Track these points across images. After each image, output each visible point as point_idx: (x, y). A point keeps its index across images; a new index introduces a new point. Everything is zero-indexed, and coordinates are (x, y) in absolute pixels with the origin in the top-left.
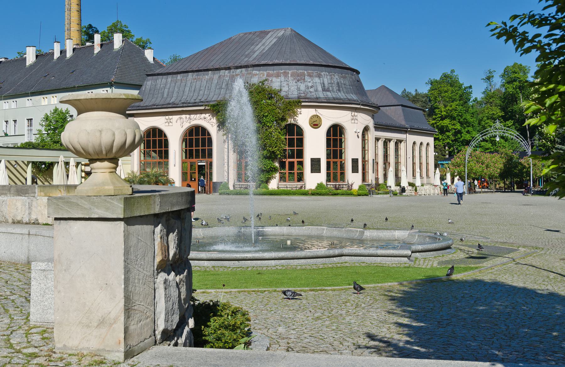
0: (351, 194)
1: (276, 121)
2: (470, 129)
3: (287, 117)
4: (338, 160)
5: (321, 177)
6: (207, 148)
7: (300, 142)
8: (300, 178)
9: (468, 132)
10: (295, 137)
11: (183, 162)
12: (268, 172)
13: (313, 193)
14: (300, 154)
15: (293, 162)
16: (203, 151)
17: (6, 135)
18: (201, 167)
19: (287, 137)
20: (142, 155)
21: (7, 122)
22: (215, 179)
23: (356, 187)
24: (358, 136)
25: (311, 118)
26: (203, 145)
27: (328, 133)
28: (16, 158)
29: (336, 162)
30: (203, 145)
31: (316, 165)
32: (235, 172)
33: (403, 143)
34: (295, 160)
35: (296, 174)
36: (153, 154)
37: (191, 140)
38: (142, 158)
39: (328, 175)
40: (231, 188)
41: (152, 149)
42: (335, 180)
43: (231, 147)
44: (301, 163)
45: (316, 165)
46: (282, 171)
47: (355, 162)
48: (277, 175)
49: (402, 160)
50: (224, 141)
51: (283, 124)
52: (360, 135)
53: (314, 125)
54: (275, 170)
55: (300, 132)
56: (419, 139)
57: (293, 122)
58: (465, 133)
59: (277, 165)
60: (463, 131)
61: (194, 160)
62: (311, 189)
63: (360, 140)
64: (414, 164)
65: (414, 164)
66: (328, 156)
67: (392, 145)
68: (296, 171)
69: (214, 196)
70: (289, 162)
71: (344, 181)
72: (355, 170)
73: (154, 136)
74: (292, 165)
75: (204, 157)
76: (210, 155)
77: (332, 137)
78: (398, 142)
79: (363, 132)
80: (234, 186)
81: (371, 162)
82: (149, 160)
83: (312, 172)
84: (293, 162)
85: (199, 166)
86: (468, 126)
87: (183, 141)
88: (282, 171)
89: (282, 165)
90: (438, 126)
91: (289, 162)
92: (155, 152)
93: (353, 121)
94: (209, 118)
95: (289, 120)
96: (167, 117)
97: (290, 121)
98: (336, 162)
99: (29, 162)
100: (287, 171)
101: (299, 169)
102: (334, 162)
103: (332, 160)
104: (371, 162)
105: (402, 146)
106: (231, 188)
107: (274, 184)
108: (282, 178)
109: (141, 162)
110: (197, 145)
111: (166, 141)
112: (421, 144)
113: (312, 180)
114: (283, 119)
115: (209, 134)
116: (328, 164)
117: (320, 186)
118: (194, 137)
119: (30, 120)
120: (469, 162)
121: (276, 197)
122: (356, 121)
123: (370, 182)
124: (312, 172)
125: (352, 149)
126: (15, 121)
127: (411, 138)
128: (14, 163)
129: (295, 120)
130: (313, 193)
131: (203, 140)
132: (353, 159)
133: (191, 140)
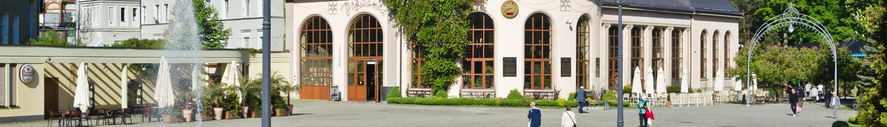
0: (555, 105)
1: (456, 9)
2: (822, 8)
3: (472, 4)
4: (542, 60)
5: (517, 83)
6: (377, 43)
7: (490, 37)
8: (490, 82)
9: (818, 12)
10: (484, 30)
11: (349, 60)
12: (447, 75)
13: (504, 104)
14: (490, 52)
15: (481, 63)
16: (373, 46)
17: (157, 23)
18: (370, 68)
19: (473, 30)
20: (304, 51)
21: (158, 6)
22: (385, 84)
23: (564, 96)
24: (571, 29)
25: (504, 5)
26: (373, 39)
27: (528, 24)
28: (104, 60)
29: (539, 63)
30: (373, 39)
31: (510, 66)
32: (410, 73)
33: (685, 31)
34: (483, 60)
35: (484, 78)
36: (321, 49)
37: (358, 33)
38: (304, 55)
39: (527, 79)
40: (404, 95)
41: (320, 43)
42: (537, 85)
43: (404, 41)
44: (491, 64)
45: (510, 66)
46: (467, 74)
47: (566, 62)
48: (459, 79)
49: (684, 54)
50: (397, 35)
51: (467, 13)
52: (574, 26)
53: (508, 14)
54: (456, 72)
55: (490, 22)
56: (711, 26)
57: (479, 10)
58: (813, 14)
59: (459, 65)
60: (811, 10)
61: (362, 58)
62: (501, 99)
63: (574, 33)
64: (703, 60)
65: (703, 60)
66: (527, 54)
67: (666, 38)
68: (484, 74)
69: (384, 104)
70: (476, 63)
71: (550, 88)
72: (565, 72)
73: (317, 27)
74: (478, 66)
75: (373, 55)
76: (381, 53)
77: (542, 30)
78: (676, 32)
79: (579, 24)
80: (407, 93)
81: (592, 63)
82: (313, 56)
83: (504, 75)
84: (481, 63)
85: (368, 66)
86: (819, 4)
87: (350, 32)
88: (467, 74)
89: (467, 66)
90: (771, 4)
91: (476, 63)
92: (324, 47)
93: (563, 8)
94: (379, 4)
95: (475, 7)
96: (331, 3)
97: (476, 8)
98: (539, 63)
99: (124, 65)
100: (472, 73)
101: (488, 71)
102: (535, 63)
103: (533, 60)
104: (592, 63)
105: (684, 36)
106: (404, 95)
107: (455, 91)
108: (466, 83)
109: (301, 60)
110: (366, 40)
111: (330, 33)
112: (716, 32)
113: (505, 86)
114: (465, 7)
115: (379, 26)
116: (527, 65)
117: (514, 94)
118: (369, 28)
119: (167, 5)
120: (753, 60)
121: (451, 108)
122: (568, 8)
123: (591, 88)
124: (504, 75)
125: (562, 45)
126: (167, 5)
127: (697, 26)
128: (102, 67)
129: (482, 7)
130: (504, 104)
131: (373, 32)
132: (562, 59)
133: (358, 33)
